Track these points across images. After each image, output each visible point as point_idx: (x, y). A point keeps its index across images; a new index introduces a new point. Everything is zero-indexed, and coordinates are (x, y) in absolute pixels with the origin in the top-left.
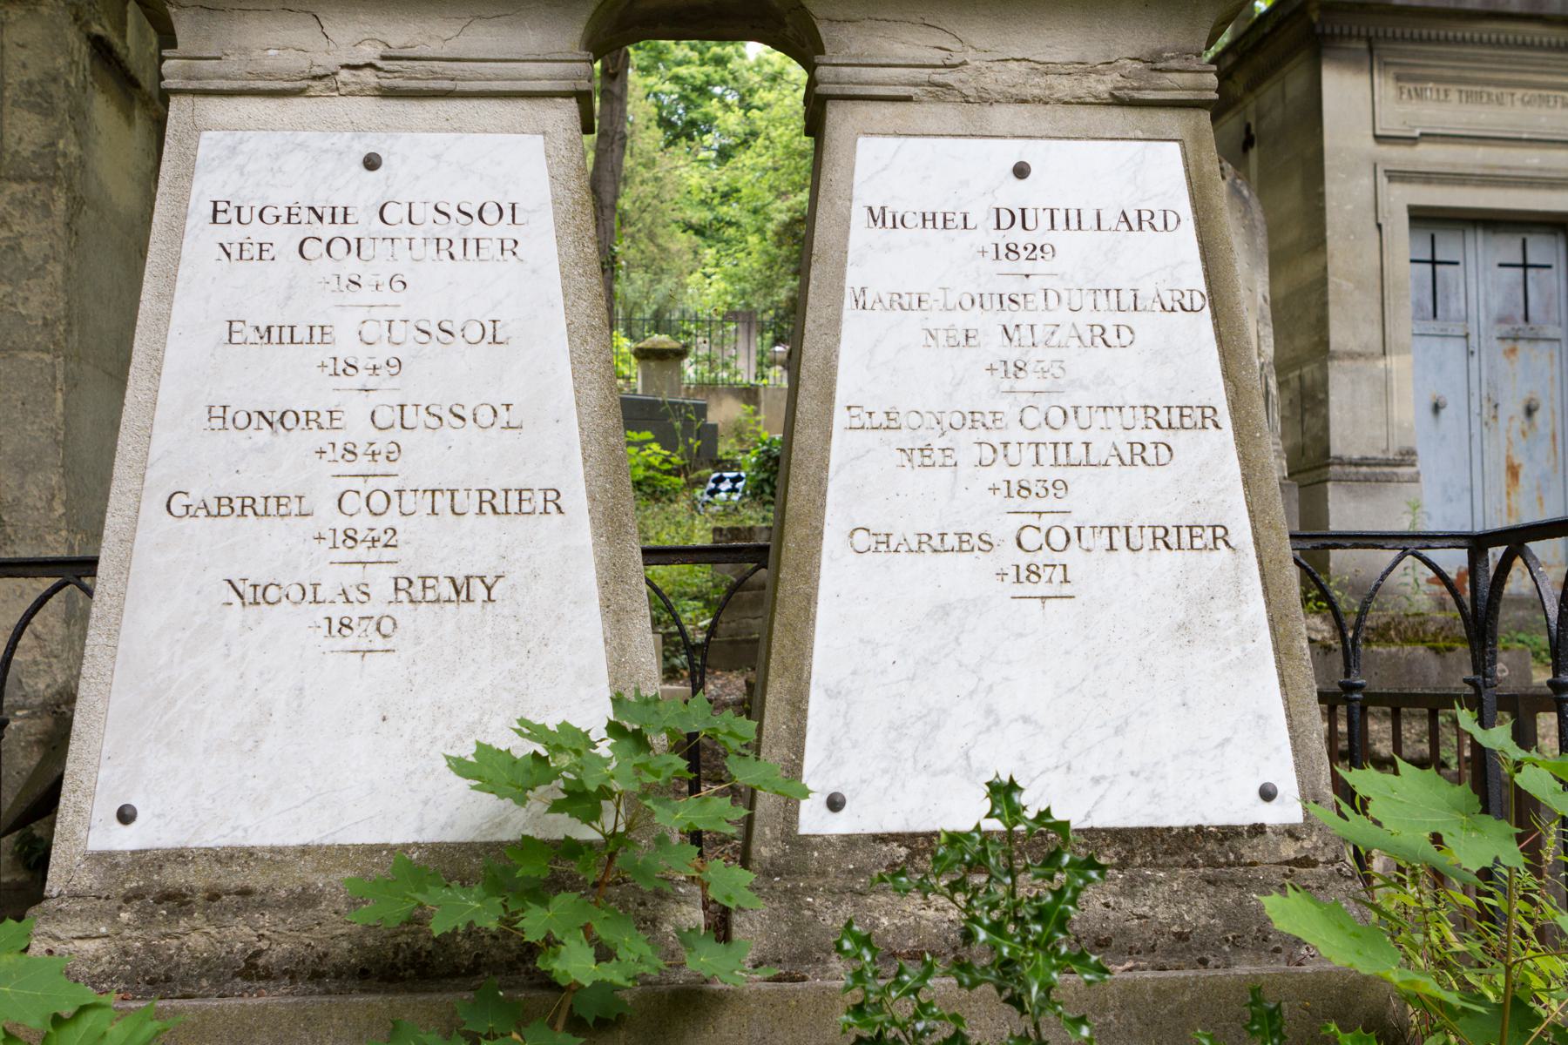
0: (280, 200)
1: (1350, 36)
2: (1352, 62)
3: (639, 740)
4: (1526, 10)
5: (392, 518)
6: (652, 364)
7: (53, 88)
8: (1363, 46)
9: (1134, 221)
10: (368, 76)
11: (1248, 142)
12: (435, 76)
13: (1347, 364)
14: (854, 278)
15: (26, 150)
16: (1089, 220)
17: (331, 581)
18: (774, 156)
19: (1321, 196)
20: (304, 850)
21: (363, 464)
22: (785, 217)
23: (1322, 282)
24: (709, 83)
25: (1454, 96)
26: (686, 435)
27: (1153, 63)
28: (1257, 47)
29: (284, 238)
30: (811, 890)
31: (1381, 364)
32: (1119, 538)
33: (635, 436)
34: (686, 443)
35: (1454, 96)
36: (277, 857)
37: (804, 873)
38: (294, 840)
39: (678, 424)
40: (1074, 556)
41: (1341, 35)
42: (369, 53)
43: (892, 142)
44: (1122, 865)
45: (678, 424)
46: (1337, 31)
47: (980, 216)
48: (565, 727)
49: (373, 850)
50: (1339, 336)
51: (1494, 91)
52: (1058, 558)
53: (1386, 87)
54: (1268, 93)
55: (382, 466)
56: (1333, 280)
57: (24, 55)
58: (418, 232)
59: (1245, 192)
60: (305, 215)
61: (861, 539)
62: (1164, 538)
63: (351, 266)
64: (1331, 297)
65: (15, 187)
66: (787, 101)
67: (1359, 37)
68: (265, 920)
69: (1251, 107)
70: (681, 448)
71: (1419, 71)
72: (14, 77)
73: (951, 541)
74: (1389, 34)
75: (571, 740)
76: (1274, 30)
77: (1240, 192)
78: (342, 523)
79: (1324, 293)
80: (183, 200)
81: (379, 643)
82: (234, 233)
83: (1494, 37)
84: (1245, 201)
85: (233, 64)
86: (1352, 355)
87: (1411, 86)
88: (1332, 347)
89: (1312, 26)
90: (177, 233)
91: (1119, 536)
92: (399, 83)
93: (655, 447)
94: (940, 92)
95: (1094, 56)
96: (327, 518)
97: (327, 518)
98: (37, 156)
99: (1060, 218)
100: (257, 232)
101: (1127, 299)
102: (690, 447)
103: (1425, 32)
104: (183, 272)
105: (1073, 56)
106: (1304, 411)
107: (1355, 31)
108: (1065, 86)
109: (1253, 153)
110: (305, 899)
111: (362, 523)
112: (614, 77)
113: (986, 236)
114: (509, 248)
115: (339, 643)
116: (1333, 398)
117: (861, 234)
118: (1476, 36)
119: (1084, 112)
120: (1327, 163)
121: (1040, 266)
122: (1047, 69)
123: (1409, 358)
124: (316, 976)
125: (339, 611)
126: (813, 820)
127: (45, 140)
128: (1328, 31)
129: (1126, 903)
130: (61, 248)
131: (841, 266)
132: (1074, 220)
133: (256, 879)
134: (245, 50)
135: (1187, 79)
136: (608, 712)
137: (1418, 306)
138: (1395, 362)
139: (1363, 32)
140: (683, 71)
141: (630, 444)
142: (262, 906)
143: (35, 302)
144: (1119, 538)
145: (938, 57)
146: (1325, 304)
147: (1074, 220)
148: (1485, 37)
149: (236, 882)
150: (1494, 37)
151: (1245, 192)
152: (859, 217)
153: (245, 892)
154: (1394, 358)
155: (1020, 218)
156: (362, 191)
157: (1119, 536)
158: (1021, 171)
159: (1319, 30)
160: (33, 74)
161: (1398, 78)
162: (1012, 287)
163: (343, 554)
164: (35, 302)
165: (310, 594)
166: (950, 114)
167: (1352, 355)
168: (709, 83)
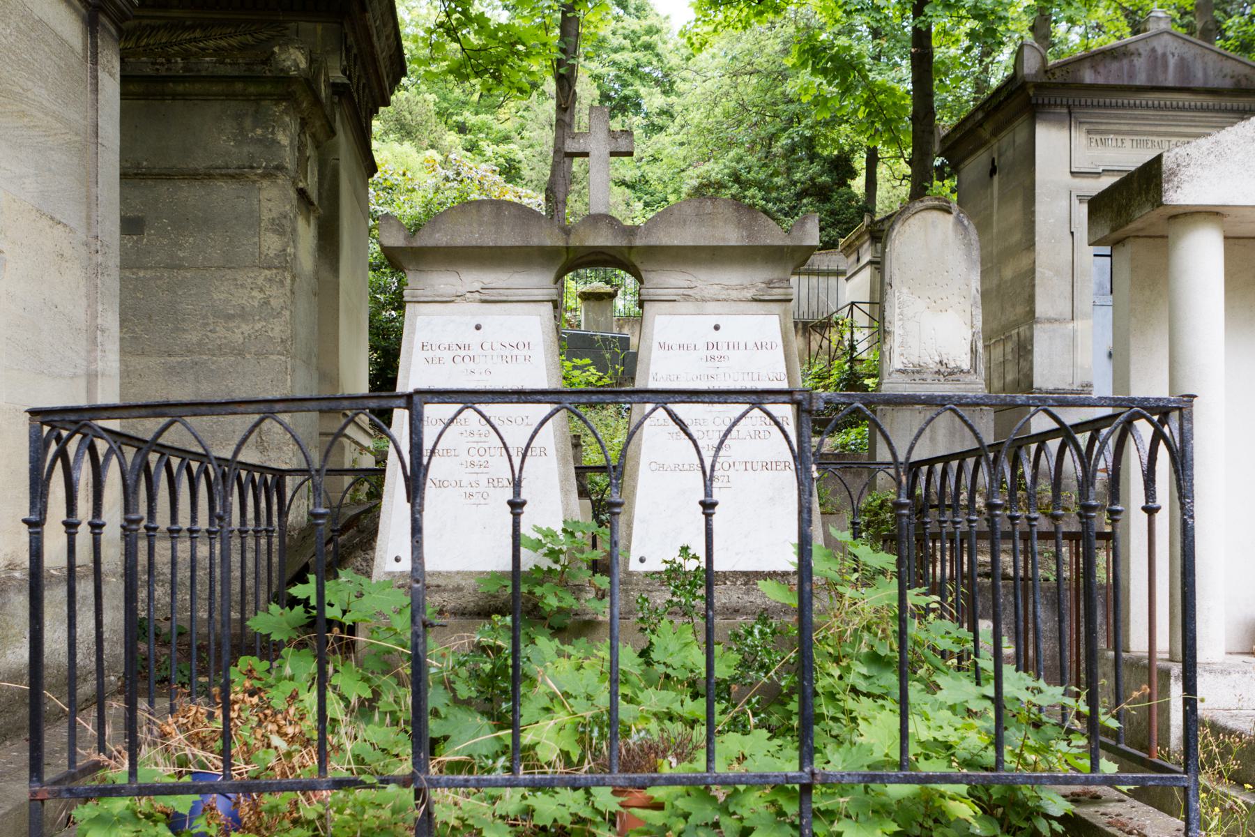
0: (446, 342)
1: (1056, 105)
2: (1057, 121)
3: (572, 534)
4: (1178, 85)
5: (487, 457)
6: (592, 304)
7: (284, 221)
8: (1065, 111)
9: (759, 346)
10: (477, 296)
11: (993, 171)
12: (500, 295)
13: (1047, 326)
14: (653, 369)
15: (272, 253)
16: (742, 346)
17: (466, 479)
18: (688, 134)
19: (1033, 213)
20: (458, 573)
21: (476, 438)
22: (695, 183)
23: (1032, 271)
24: (638, 66)
25: (1128, 143)
26: (614, 362)
27: (769, 284)
28: (997, 108)
29: (447, 355)
30: (633, 590)
31: (1070, 326)
32: (749, 466)
33: (578, 362)
34: (613, 368)
35: (1128, 143)
36: (448, 575)
37: (630, 583)
38: (454, 569)
39: (608, 356)
40: (732, 472)
41: (1049, 105)
42: (477, 286)
43: (669, 317)
44: (746, 584)
45: (608, 356)
46: (1046, 101)
47: (701, 346)
48: (548, 529)
49: (482, 573)
50: (1041, 308)
51: (1156, 139)
52: (726, 473)
53: (1080, 137)
54: (1005, 138)
55: (483, 439)
56: (1039, 270)
57: (270, 205)
58: (495, 353)
59: (966, 222)
60: (455, 347)
61: (654, 466)
62: (766, 466)
63: (471, 366)
64: (1037, 281)
65: (267, 272)
66: (698, 91)
67: (1062, 105)
68: (446, 595)
69: (995, 147)
70: (610, 372)
71: (1103, 127)
72: (266, 216)
73: (687, 467)
74: (1083, 102)
75: (549, 534)
76: (1006, 99)
77: (962, 222)
78: (469, 459)
79: (1033, 279)
80: (411, 342)
81: (483, 501)
82: (429, 354)
83: (1156, 103)
84: (965, 228)
85: (428, 292)
86: (1050, 321)
87: (1098, 137)
88: (1037, 315)
89: (1030, 98)
90: (410, 354)
91: (749, 465)
92: (488, 298)
93: (592, 370)
94: (687, 298)
95: (746, 282)
96: (464, 457)
97: (464, 457)
98: (277, 256)
99: (731, 346)
100: (438, 353)
101: (756, 376)
102: (616, 371)
103: (1108, 101)
104: (412, 369)
105: (739, 282)
106: (1020, 356)
107: (1059, 101)
108: (734, 294)
109: (996, 178)
110: (459, 589)
111: (476, 459)
112: (565, 110)
113: (703, 352)
114: (527, 359)
115: (468, 501)
116: (1036, 349)
117: (656, 353)
118: (1144, 103)
119: (741, 304)
120: (1037, 191)
121: (723, 364)
122: (728, 288)
123: (1090, 322)
124: (463, 614)
125: (469, 490)
126: (634, 566)
127: (280, 248)
128: (1040, 101)
129: (746, 597)
130: (289, 303)
131: (648, 364)
132: (736, 346)
133: (442, 582)
134: (432, 285)
135: (781, 291)
136: (562, 526)
137: (1100, 286)
138: (1079, 324)
139: (1065, 102)
140: (618, 57)
141: (575, 368)
142: (444, 590)
143: (277, 329)
144: (749, 466)
145: (686, 284)
146: (1034, 286)
147: (736, 346)
148: (1150, 103)
149: (435, 583)
150: (1156, 103)
151: (966, 222)
152: (655, 346)
153: (438, 586)
154: (1080, 323)
155: (716, 346)
156: (474, 338)
157: (749, 465)
158: (717, 328)
159: (1034, 101)
160: (274, 214)
161: (1089, 132)
162: (712, 372)
163: (469, 470)
164: (277, 329)
165: (459, 484)
166: (690, 306)
167: (1050, 321)
168: (638, 66)
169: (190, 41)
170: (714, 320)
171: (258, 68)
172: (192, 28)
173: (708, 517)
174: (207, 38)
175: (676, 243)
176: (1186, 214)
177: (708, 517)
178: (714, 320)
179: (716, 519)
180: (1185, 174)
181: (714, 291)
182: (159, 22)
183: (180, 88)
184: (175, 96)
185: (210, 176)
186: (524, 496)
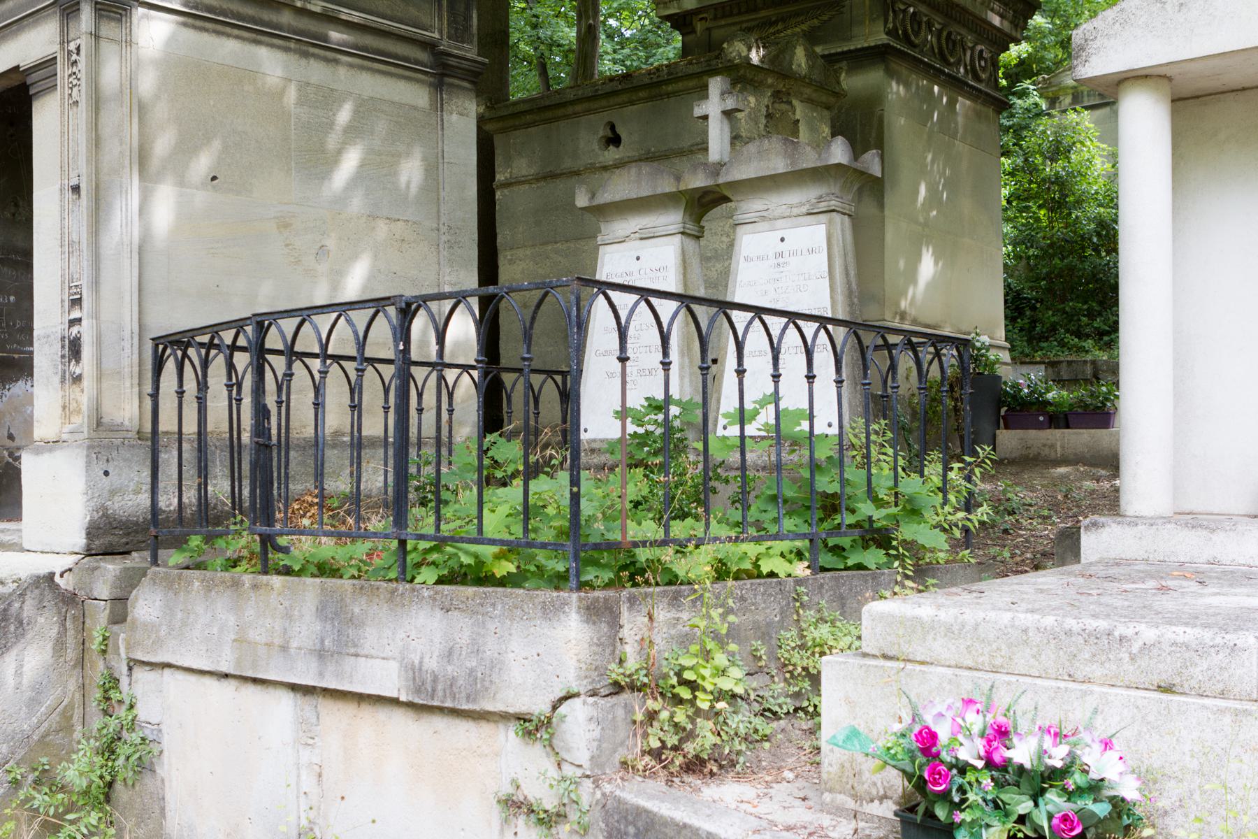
14: (739, 279)
47: (771, 255)
94: (763, 218)
108: (795, 211)
132: (794, 254)
147: (794, 254)
152: (742, 259)
155: (781, 255)
166: (765, 225)
169: (774, 34)
170: (780, 234)
171: (714, 62)
172: (776, 23)
173: (776, 383)
174: (786, 28)
175: (744, 177)
176: (97, 222)
177: (776, 383)
178: (780, 234)
179: (815, 385)
180: (1093, 45)
181: (783, 210)
182: (753, 23)
183: (670, 88)
184: (669, 95)
185: (691, 152)
186: (781, 371)
